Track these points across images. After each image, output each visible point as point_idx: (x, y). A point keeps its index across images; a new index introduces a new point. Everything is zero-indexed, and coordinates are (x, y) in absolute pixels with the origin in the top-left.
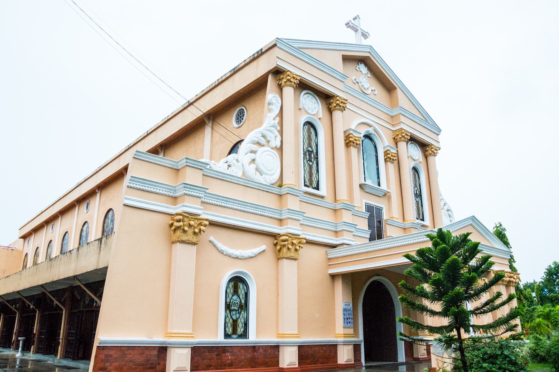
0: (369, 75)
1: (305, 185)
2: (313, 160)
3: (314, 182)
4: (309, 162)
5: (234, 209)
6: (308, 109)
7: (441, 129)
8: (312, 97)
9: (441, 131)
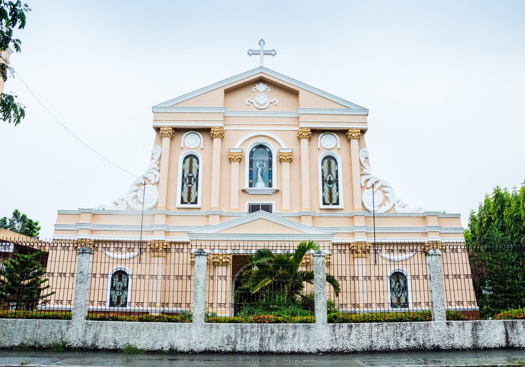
0: (269, 90)
1: (324, 204)
2: (192, 183)
3: (334, 199)
4: (188, 185)
5: (360, 232)
6: (326, 146)
7: (367, 108)
8: (330, 135)
9: (369, 111)
